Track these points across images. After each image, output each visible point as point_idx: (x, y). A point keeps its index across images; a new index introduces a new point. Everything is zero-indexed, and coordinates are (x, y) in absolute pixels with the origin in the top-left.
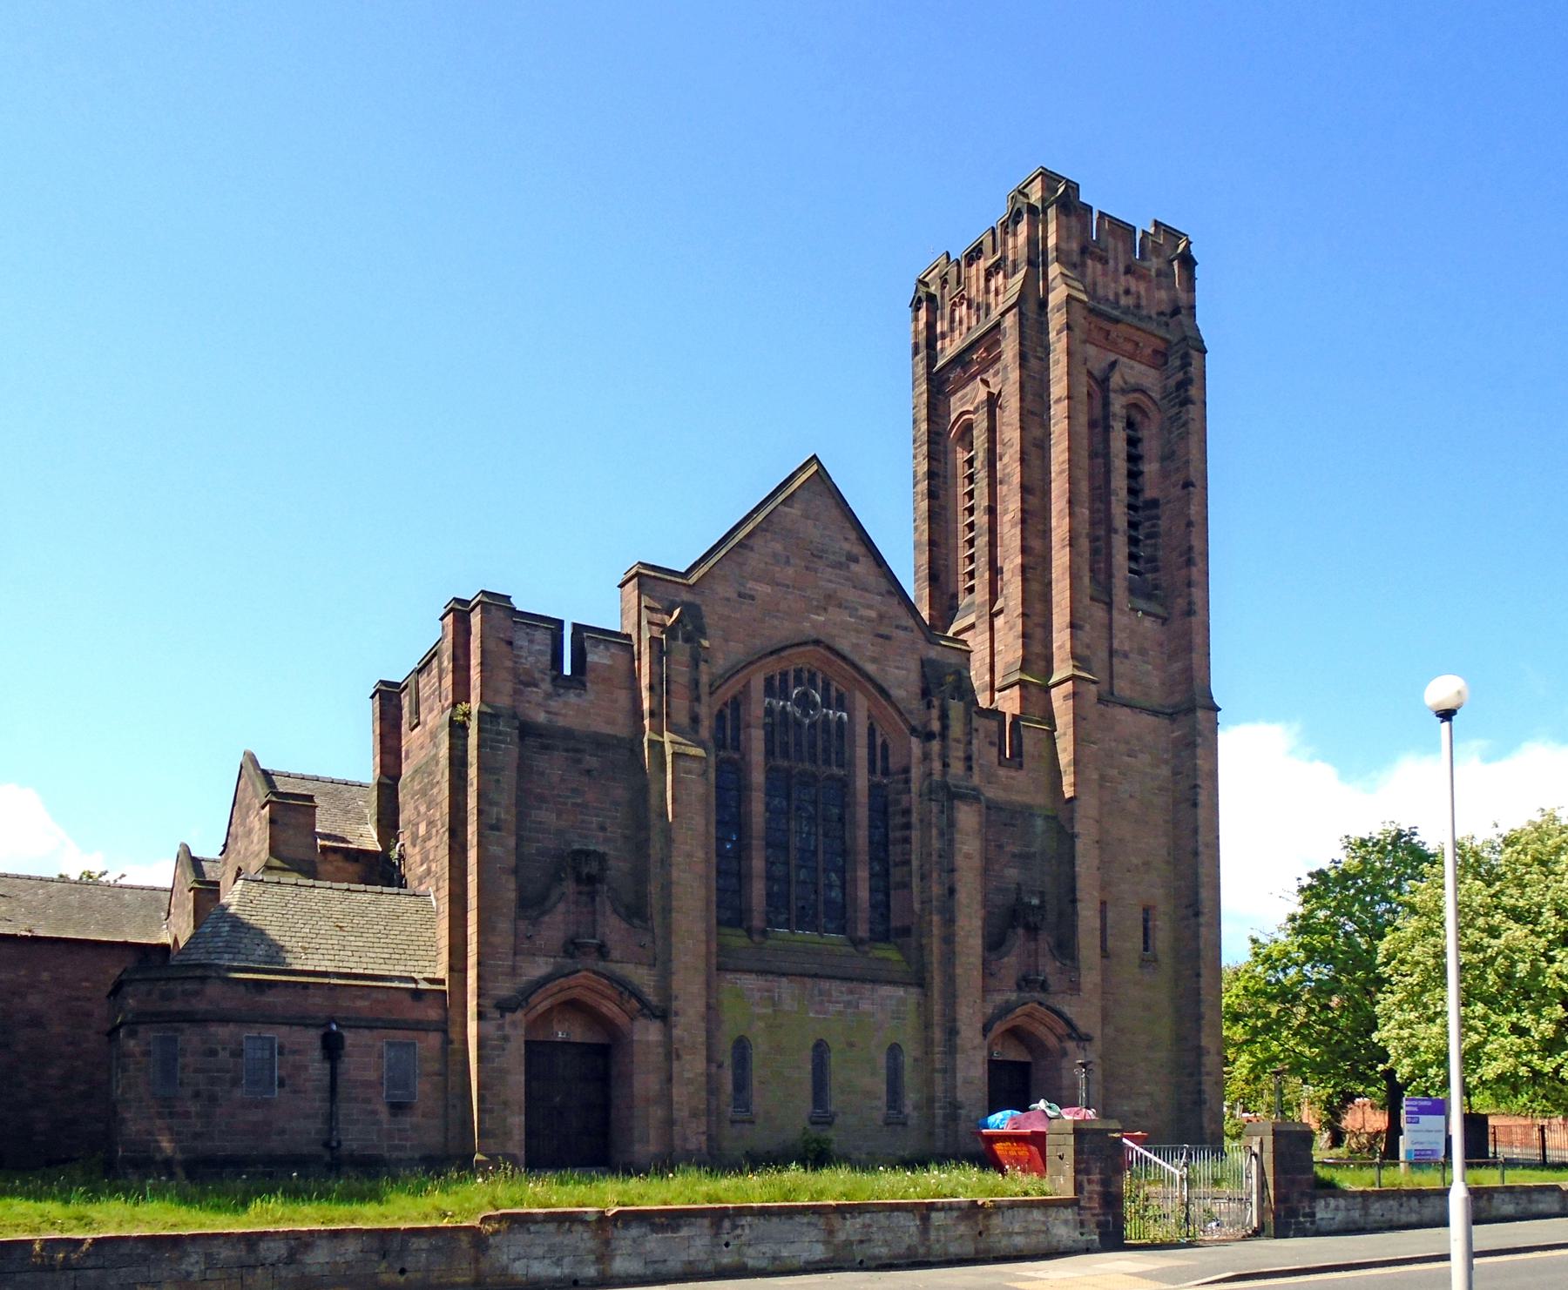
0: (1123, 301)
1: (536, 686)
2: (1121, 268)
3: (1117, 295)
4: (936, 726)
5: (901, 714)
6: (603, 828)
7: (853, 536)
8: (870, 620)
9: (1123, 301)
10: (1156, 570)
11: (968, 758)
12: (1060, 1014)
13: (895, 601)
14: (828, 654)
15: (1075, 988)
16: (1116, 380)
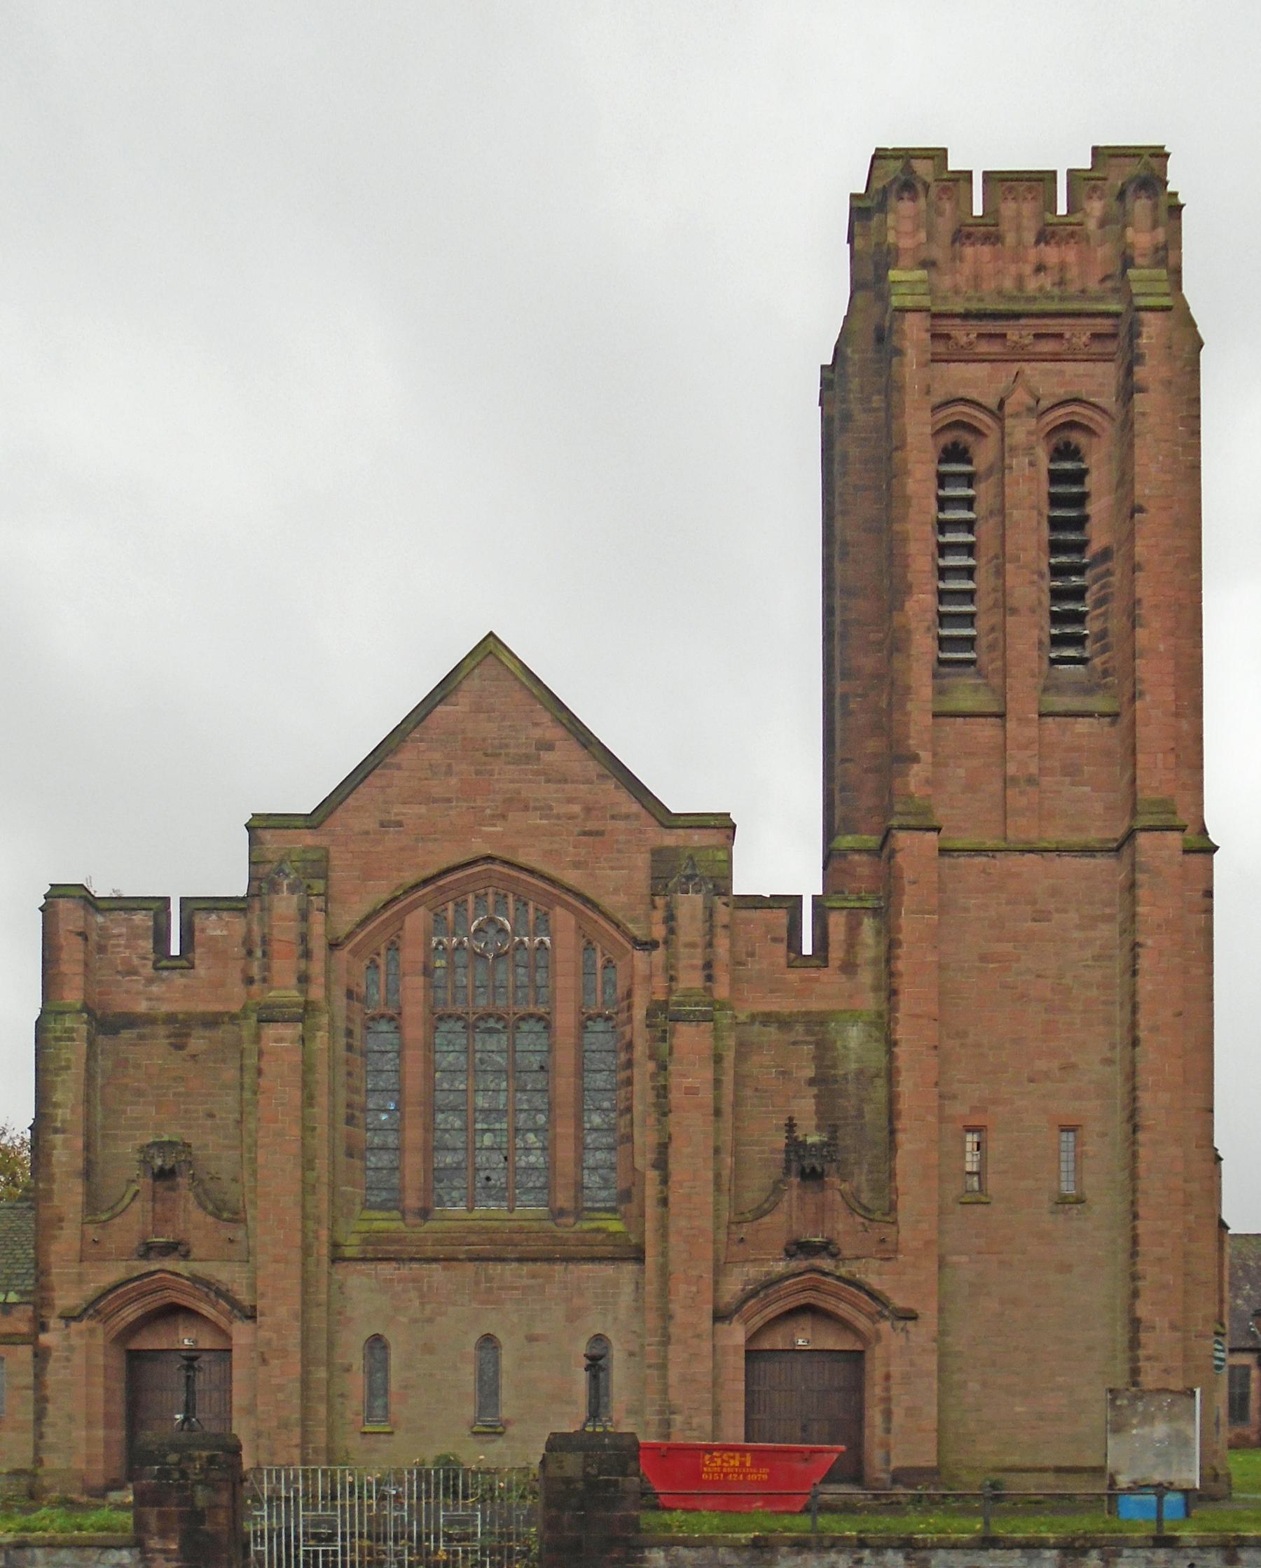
0: (1032, 285)
1: (136, 973)
2: (1030, 237)
3: (1020, 280)
4: (659, 932)
5: (618, 926)
6: (211, 1116)
7: (546, 718)
8: (572, 817)
9: (1032, 285)
10: (1105, 649)
11: (708, 965)
12: (859, 1286)
13: (610, 785)
14: (506, 870)
15: (888, 1251)
16: (1020, 398)
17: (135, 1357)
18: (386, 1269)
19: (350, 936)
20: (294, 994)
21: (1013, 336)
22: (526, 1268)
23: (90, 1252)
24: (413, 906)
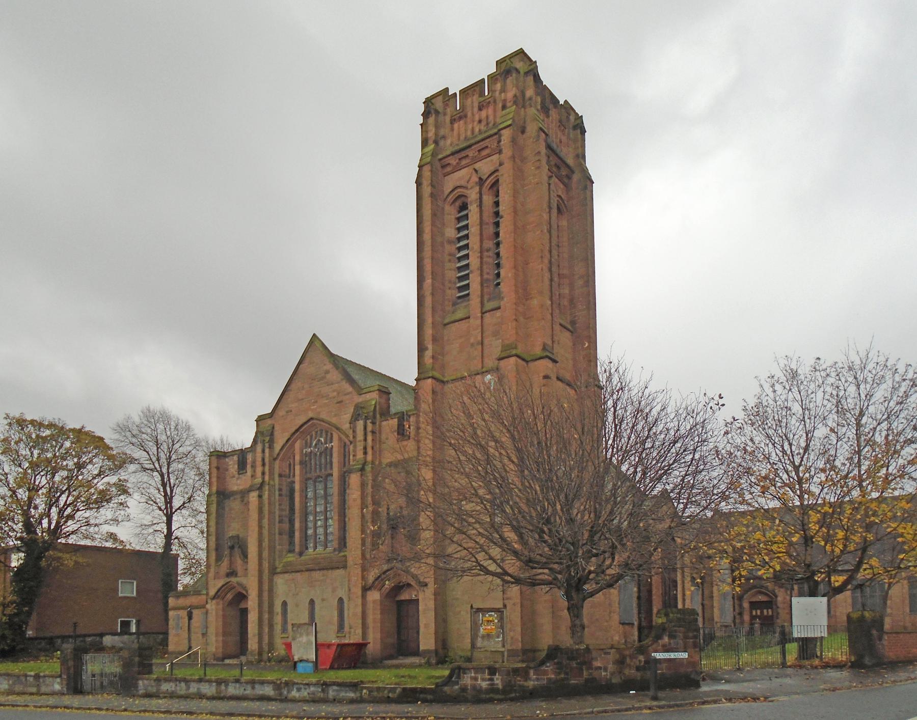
2: (476, 109)
17: (400, 603)
18: (286, 576)
22: (322, 572)
24: (295, 442)
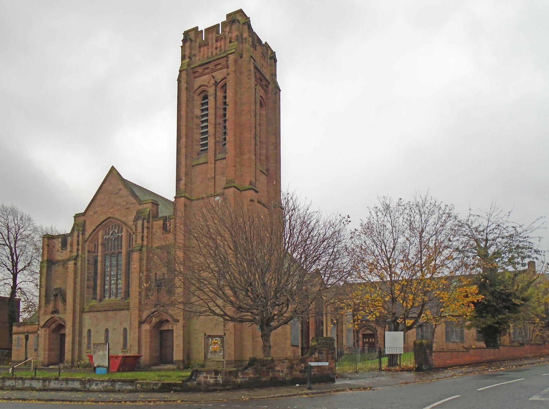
2: (214, 41)
7: (120, 183)
17: (162, 332)
19: (88, 239)
20: (155, 245)
21: (210, 67)
23: (45, 314)
